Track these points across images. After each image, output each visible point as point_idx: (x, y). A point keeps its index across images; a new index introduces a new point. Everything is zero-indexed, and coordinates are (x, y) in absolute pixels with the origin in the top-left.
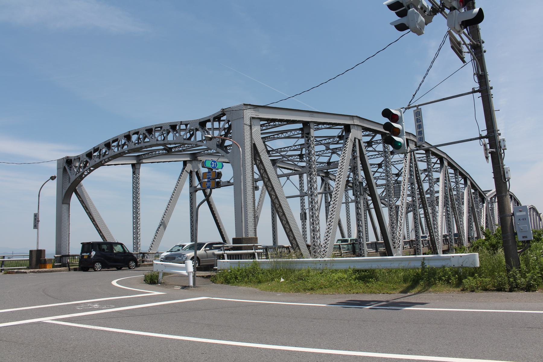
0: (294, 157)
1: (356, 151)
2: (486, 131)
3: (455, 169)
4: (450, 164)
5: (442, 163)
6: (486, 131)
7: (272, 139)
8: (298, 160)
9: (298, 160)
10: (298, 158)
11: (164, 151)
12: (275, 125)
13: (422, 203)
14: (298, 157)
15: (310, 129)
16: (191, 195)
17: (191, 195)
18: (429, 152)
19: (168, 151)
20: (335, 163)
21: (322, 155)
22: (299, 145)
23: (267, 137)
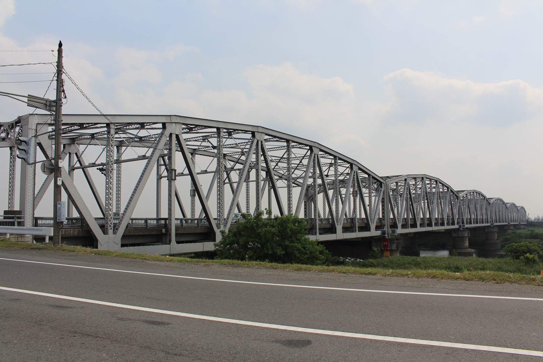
0: (204, 150)
1: (315, 160)
2: (368, 197)
3: (443, 185)
4: (481, 195)
5: (351, 168)
6: (368, 197)
7: (210, 137)
8: (227, 136)
9: (227, 136)
10: (227, 135)
11: (187, 130)
12: (212, 137)
13: (56, 115)
14: (227, 134)
15: (110, 129)
16: (158, 181)
17: (158, 181)
18: (370, 176)
19: (190, 131)
20: (209, 136)
21: (247, 141)
22: (201, 136)
23: (207, 136)
